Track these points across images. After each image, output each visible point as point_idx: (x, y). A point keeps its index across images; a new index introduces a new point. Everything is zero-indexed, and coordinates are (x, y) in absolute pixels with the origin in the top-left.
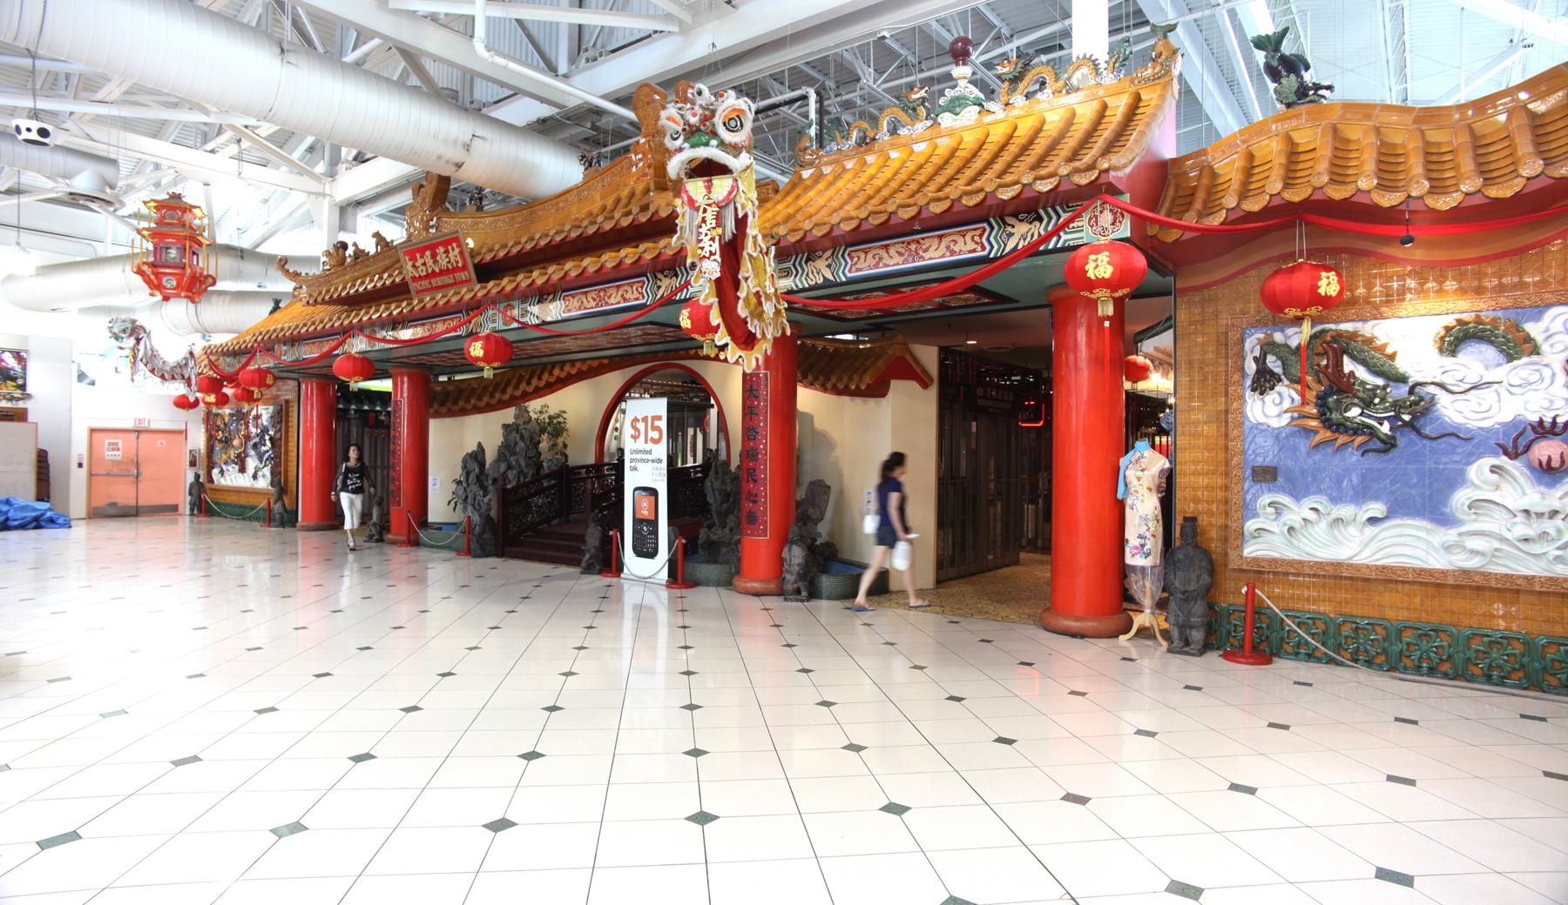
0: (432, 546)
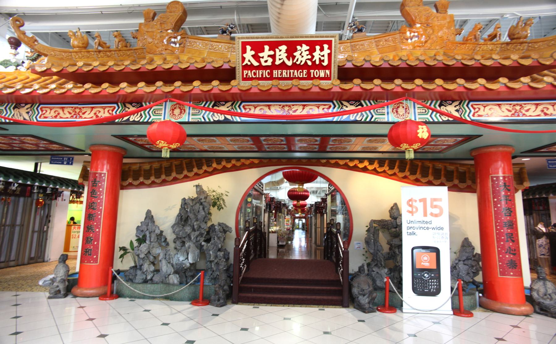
0: (144, 297)
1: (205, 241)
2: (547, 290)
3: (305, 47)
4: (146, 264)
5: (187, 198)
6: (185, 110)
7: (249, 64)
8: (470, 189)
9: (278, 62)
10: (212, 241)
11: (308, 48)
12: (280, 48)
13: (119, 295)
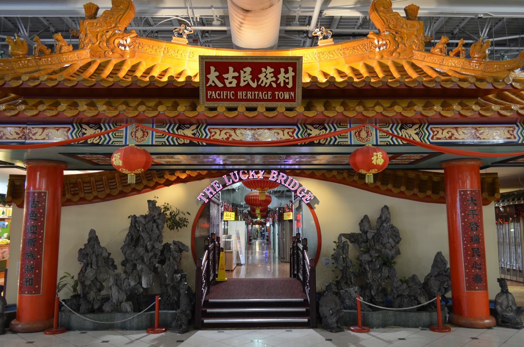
1: (159, 263)
2: (509, 303)
3: (270, 70)
4: (92, 292)
5: (138, 216)
6: (147, 133)
7: (213, 85)
8: (441, 200)
9: (242, 84)
10: (167, 262)
11: (273, 70)
12: (245, 69)
13: (67, 328)
